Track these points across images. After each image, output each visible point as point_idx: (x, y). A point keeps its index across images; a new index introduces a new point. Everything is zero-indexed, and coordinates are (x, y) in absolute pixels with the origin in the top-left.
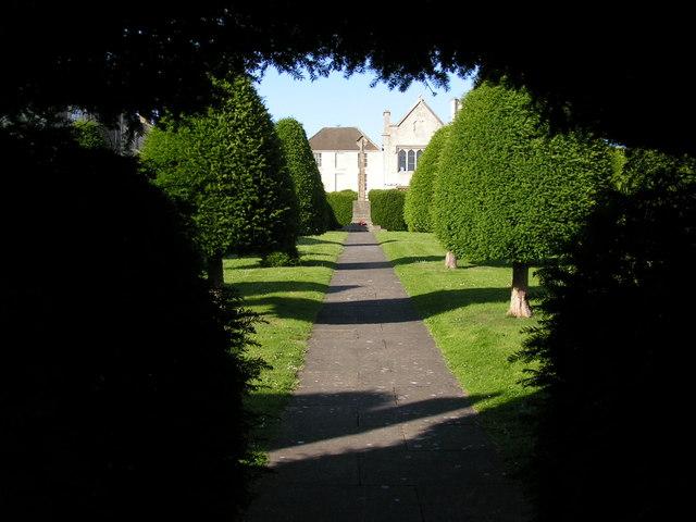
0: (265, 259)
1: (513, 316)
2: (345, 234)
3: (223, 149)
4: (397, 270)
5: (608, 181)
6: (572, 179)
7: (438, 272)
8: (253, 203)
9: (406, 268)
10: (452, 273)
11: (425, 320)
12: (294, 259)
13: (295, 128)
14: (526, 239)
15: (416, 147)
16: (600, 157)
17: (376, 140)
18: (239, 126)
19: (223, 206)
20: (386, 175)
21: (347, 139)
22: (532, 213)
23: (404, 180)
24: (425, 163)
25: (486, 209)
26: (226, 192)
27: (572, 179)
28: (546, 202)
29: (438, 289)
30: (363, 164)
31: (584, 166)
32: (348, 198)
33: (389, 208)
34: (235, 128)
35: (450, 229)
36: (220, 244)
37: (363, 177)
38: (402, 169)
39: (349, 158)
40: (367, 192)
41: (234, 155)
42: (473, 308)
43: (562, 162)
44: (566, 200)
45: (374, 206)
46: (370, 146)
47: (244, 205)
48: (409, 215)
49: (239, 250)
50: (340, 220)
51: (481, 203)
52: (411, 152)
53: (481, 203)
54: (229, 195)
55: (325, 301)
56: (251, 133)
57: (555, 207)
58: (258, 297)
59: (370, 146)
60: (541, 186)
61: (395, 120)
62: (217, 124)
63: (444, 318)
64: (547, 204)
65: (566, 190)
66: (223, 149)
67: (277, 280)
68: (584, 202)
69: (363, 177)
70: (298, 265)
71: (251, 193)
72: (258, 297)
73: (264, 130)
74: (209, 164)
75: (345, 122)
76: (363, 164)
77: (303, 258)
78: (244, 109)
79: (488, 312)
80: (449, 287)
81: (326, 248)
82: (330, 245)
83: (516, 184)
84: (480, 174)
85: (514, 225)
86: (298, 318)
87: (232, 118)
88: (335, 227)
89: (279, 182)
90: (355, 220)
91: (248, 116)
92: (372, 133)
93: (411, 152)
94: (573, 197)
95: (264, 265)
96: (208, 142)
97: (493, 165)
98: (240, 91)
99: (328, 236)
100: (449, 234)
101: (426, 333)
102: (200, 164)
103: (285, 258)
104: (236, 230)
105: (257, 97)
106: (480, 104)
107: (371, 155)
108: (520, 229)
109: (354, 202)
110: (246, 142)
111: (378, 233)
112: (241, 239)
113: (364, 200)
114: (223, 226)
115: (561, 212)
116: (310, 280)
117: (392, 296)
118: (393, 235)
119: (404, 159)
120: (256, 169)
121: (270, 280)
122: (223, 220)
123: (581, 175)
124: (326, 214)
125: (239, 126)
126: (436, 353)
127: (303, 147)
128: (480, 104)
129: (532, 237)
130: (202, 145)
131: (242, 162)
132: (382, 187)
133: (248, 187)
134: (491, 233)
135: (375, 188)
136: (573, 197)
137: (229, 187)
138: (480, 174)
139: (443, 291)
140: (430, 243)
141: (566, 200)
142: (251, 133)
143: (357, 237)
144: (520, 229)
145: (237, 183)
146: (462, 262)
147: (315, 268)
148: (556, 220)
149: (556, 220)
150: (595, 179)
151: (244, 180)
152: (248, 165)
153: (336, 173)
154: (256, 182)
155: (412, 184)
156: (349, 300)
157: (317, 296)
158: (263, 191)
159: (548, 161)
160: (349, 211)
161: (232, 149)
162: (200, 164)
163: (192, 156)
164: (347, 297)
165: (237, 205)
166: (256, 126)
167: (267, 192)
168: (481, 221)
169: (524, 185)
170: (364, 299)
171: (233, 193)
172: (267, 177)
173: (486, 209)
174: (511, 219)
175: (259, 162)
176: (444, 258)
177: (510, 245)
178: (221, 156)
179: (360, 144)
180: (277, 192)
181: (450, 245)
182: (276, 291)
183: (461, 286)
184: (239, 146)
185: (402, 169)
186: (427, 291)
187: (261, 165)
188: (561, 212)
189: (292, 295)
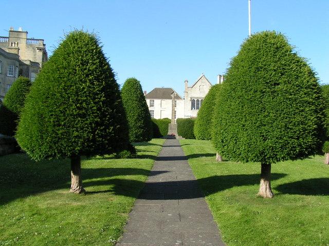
0: (118, 154)
1: (261, 197)
2: (164, 140)
3: (78, 88)
4: (189, 161)
5: (324, 113)
6: (302, 111)
7: (213, 164)
8: (97, 123)
9: (194, 160)
10: (219, 164)
11: (206, 198)
12: (133, 154)
13: (134, 85)
14: (273, 149)
15: (200, 98)
16: (318, 98)
17: (181, 94)
18: (90, 74)
19: (77, 124)
20: (185, 111)
21: (165, 93)
22: (277, 133)
23: (194, 114)
24: (207, 106)
25: (247, 130)
26: (79, 115)
27: (302, 111)
28: (286, 126)
29: (213, 175)
30: (174, 106)
31: (309, 103)
32: (166, 122)
33: (187, 128)
34: (87, 76)
35: (223, 142)
36: (74, 149)
37: (174, 112)
38: (193, 109)
39: (167, 103)
40: (176, 120)
41: (85, 92)
42: (236, 190)
43: (295, 100)
44: (298, 124)
45: (179, 126)
46: (178, 97)
47: (91, 124)
48: (196, 131)
49: (89, 155)
50: (162, 133)
51: (244, 126)
52: (198, 101)
53: (244, 126)
54: (81, 118)
55: (147, 181)
56: (97, 79)
57: (291, 129)
58: (106, 179)
59: (178, 97)
60: (282, 116)
61: (190, 85)
62: (75, 73)
63: (218, 196)
64: (286, 127)
65: (298, 118)
66: (78, 88)
67: (121, 167)
68: (309, 126)
69: (174, 112)
70: (135, 158)
71: (96, 117)
72: (106, 179)
73: (106, 78)
74: (69, 97)
75: (167, 86)
76: (174, 106)
77: (139, 154)
78: (94, 64)
79: (245, 192)
80: (219, 174)
81: (152, 148)
82: (156, 146)
83: (266, 114)
84: (243, 107)
85: (265, 140)
86: (127, 195)
87: (85, 69)
88: (158, 135)
89: (113, 110)
90: (169, 133)
91: (96, 68)
92: (179, 90)
93: (198, 101)
94: (303, 123)
95: (118, 157)
96: (69, 84)
97: (251, 101)
98: (92, 53)
99: (153, 141)
100: (222, 144)
101: (207, 208)
102: (64, 97)
103: (129, 154)
104: (85, 140)
105: (104, 58)
106: (242, 64)
107: (178, 101)
108: (269, 142)
109: (169, 124)
110: (94, 84)
111: (181, 140)
112: (88, 146)
113: (174, 123)
114: (76, 137)
115: (295, 132)
116: (140, 167)
117: (186, 179)
118: (188, 141)
119: (194, 104)
120: (99, 101)
121: (117, 167)
122: (76, 134)
123: (307, 109)
124: (153, 129)
125: (90, 74)
126: (214, 225)
127: (140, 93)
128: (242, 64)
129: (276, 148)
130: (65, 86)
131: (90, 97)
132: (183, 117)
133: (93, 113)
134: (250, 145)
135: (180, 117)
136: (303, 123)
137: (81, 112)
138: (243, 107)
139: (216, 177)
140: (208, 146)
141: (298, 124)
142: (97, 79)
143: (170, 142)
144: (269, 142)
145: (87, 110)
146: (224, 158)
147: (145, 160)
148: (292, 137)
149: (292, 137)
150: (316, 111)
151: (91, 108)
152: (94, 99)
153: (160, 110)
154: (99, 109)
155: (198, 114)
156: (161, 181)
157: (142, 178)
158: (103, 115)
159: (287, 99)
160: (166, 129)
161: (84, 88)
162: (64, 97)
163: (58, 92)
164: (160, 179)
165: (86, 124)
166: (101, 75)
167: (106, 116)
168: (243, 138)
169: (271, 115)
170: (170, 180)
171: (83, 116)
172: (107, 106)
173: (247, 130)
174: (263, 136)
175: (101, 97)
176: (215, 155)
177: (262, 153)
178: (77, 93)
179: (172, 96)
180: (112, 116)
181: (223, 152)
182: (118, 175)
183: (226, 173)
184: (89, 87)
185: (193, 109)
186: (206, 176)
187: (102, 99)
188: (295, 132)
189: (128, 177)
